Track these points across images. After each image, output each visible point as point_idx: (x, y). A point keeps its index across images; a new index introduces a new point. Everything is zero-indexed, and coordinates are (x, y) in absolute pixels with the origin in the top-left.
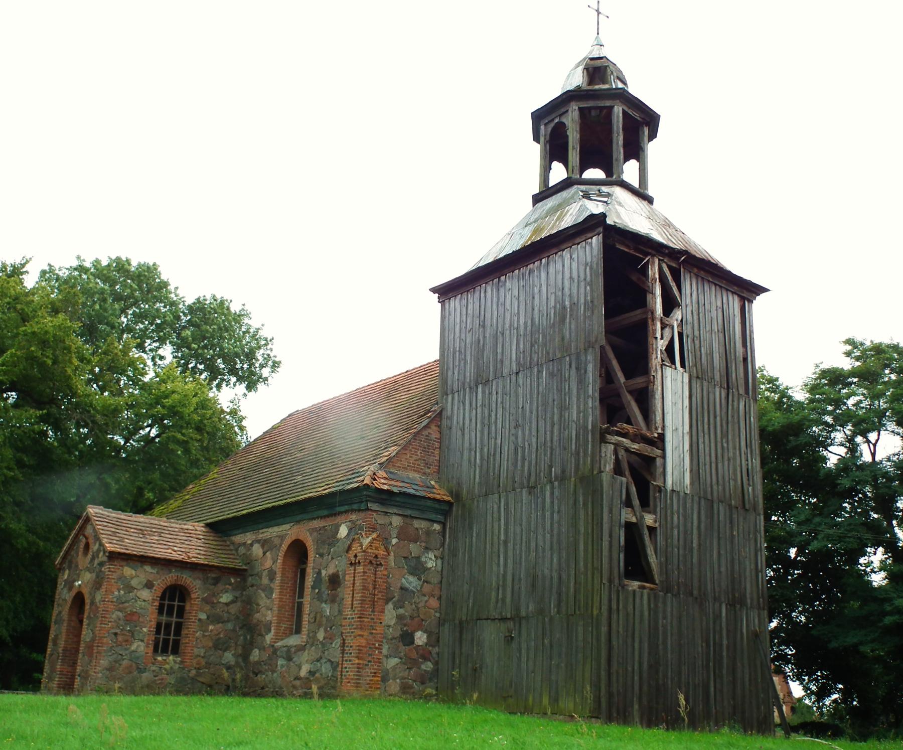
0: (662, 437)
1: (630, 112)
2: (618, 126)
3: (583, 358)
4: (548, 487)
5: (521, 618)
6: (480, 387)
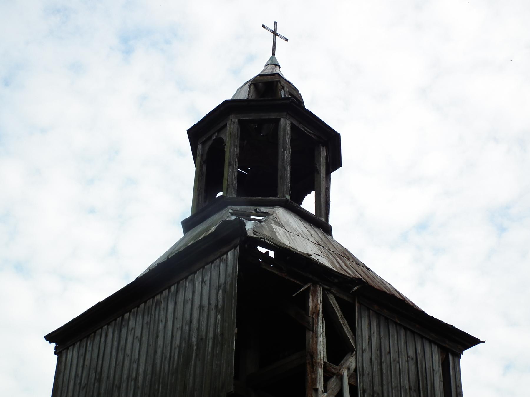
1: (301, 127)
2: (284, 140)
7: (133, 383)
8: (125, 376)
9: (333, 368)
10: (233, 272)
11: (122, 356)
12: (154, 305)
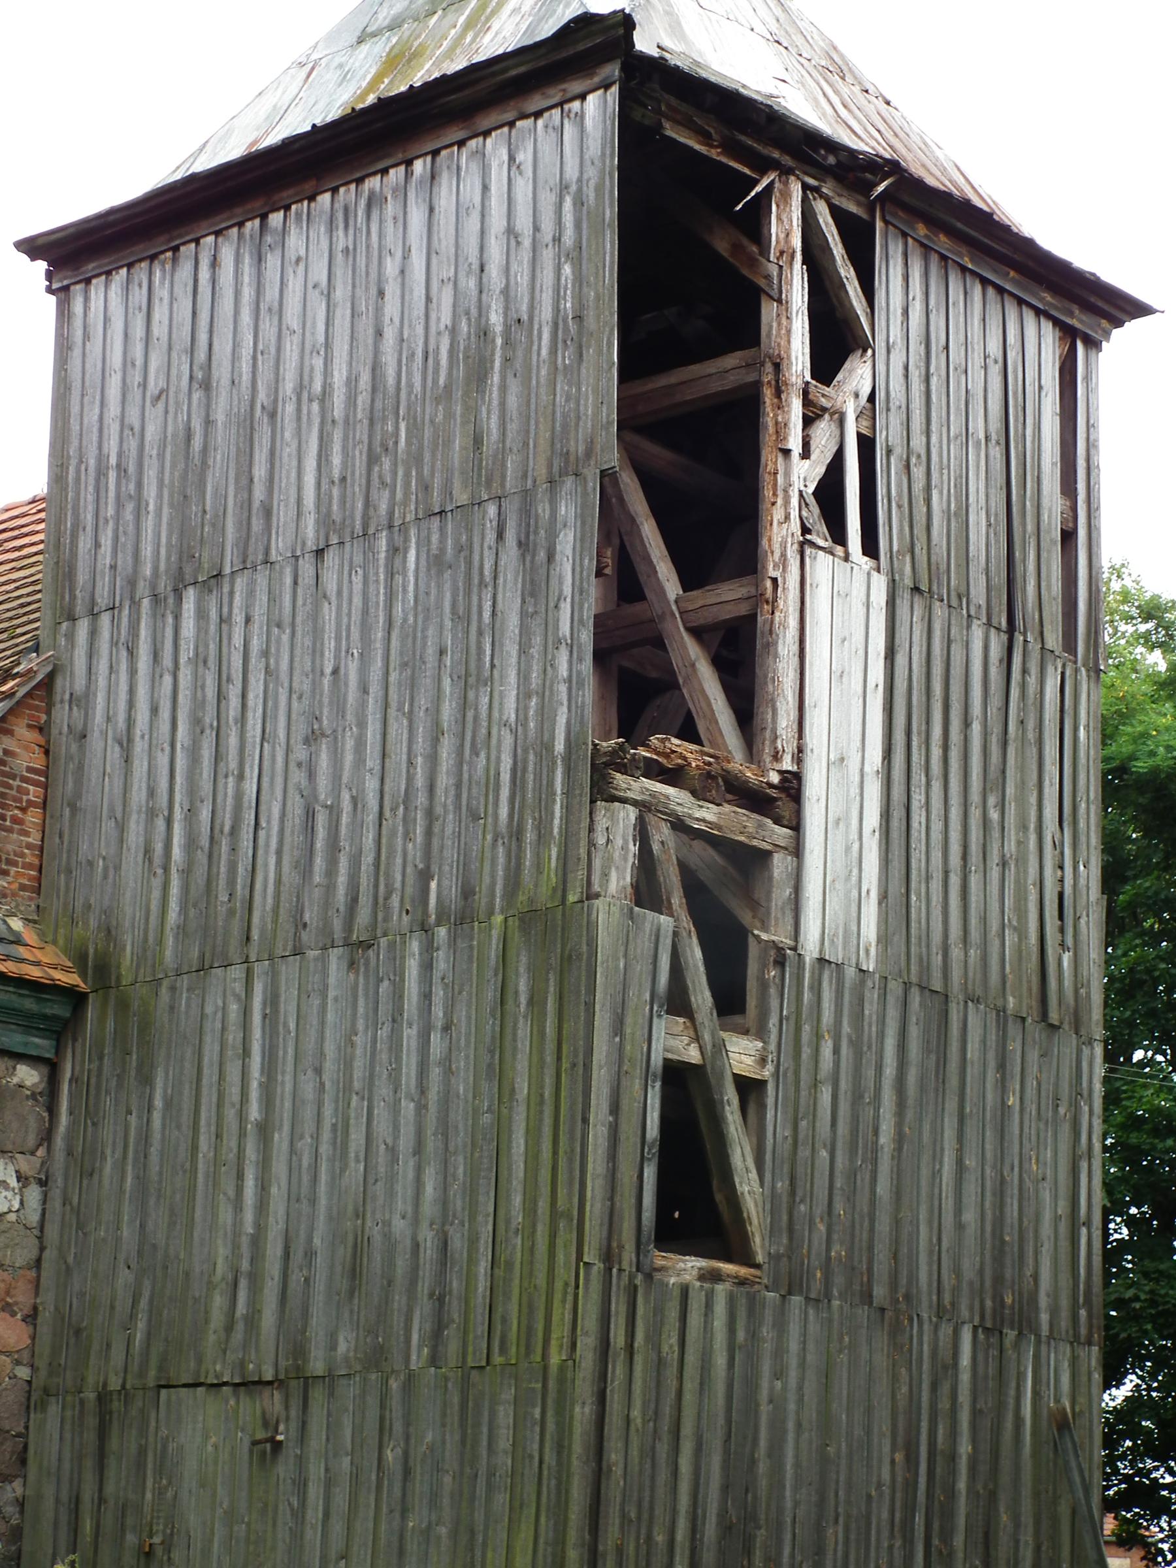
0: (793, 785)
4: (415, 946)
5: (307, 1381)
6: (190, 597)
7: (315, 407)
8: (289, 386)
9: (823, 395)
10: (603, 154)
11: (275, 330)
12: (363, 203)
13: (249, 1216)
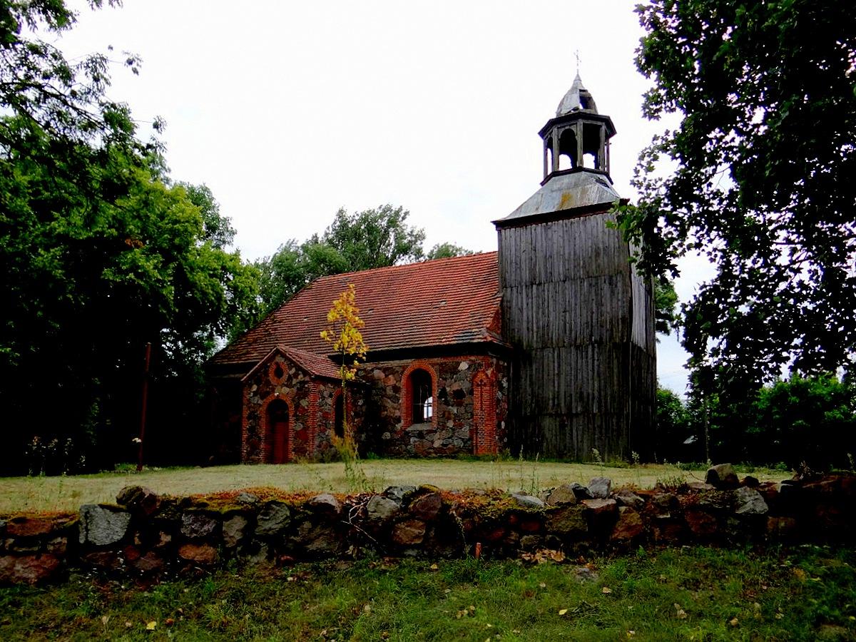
3: (614, 278)
4: (590, 347)
6: (534, 286)
13: (556, 389)
